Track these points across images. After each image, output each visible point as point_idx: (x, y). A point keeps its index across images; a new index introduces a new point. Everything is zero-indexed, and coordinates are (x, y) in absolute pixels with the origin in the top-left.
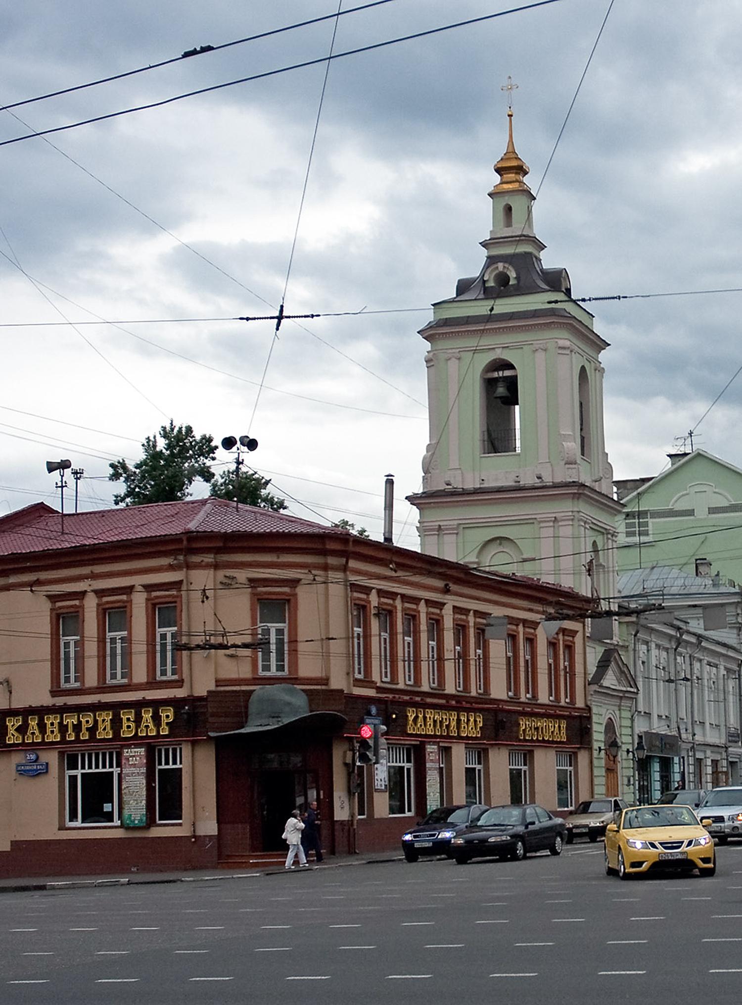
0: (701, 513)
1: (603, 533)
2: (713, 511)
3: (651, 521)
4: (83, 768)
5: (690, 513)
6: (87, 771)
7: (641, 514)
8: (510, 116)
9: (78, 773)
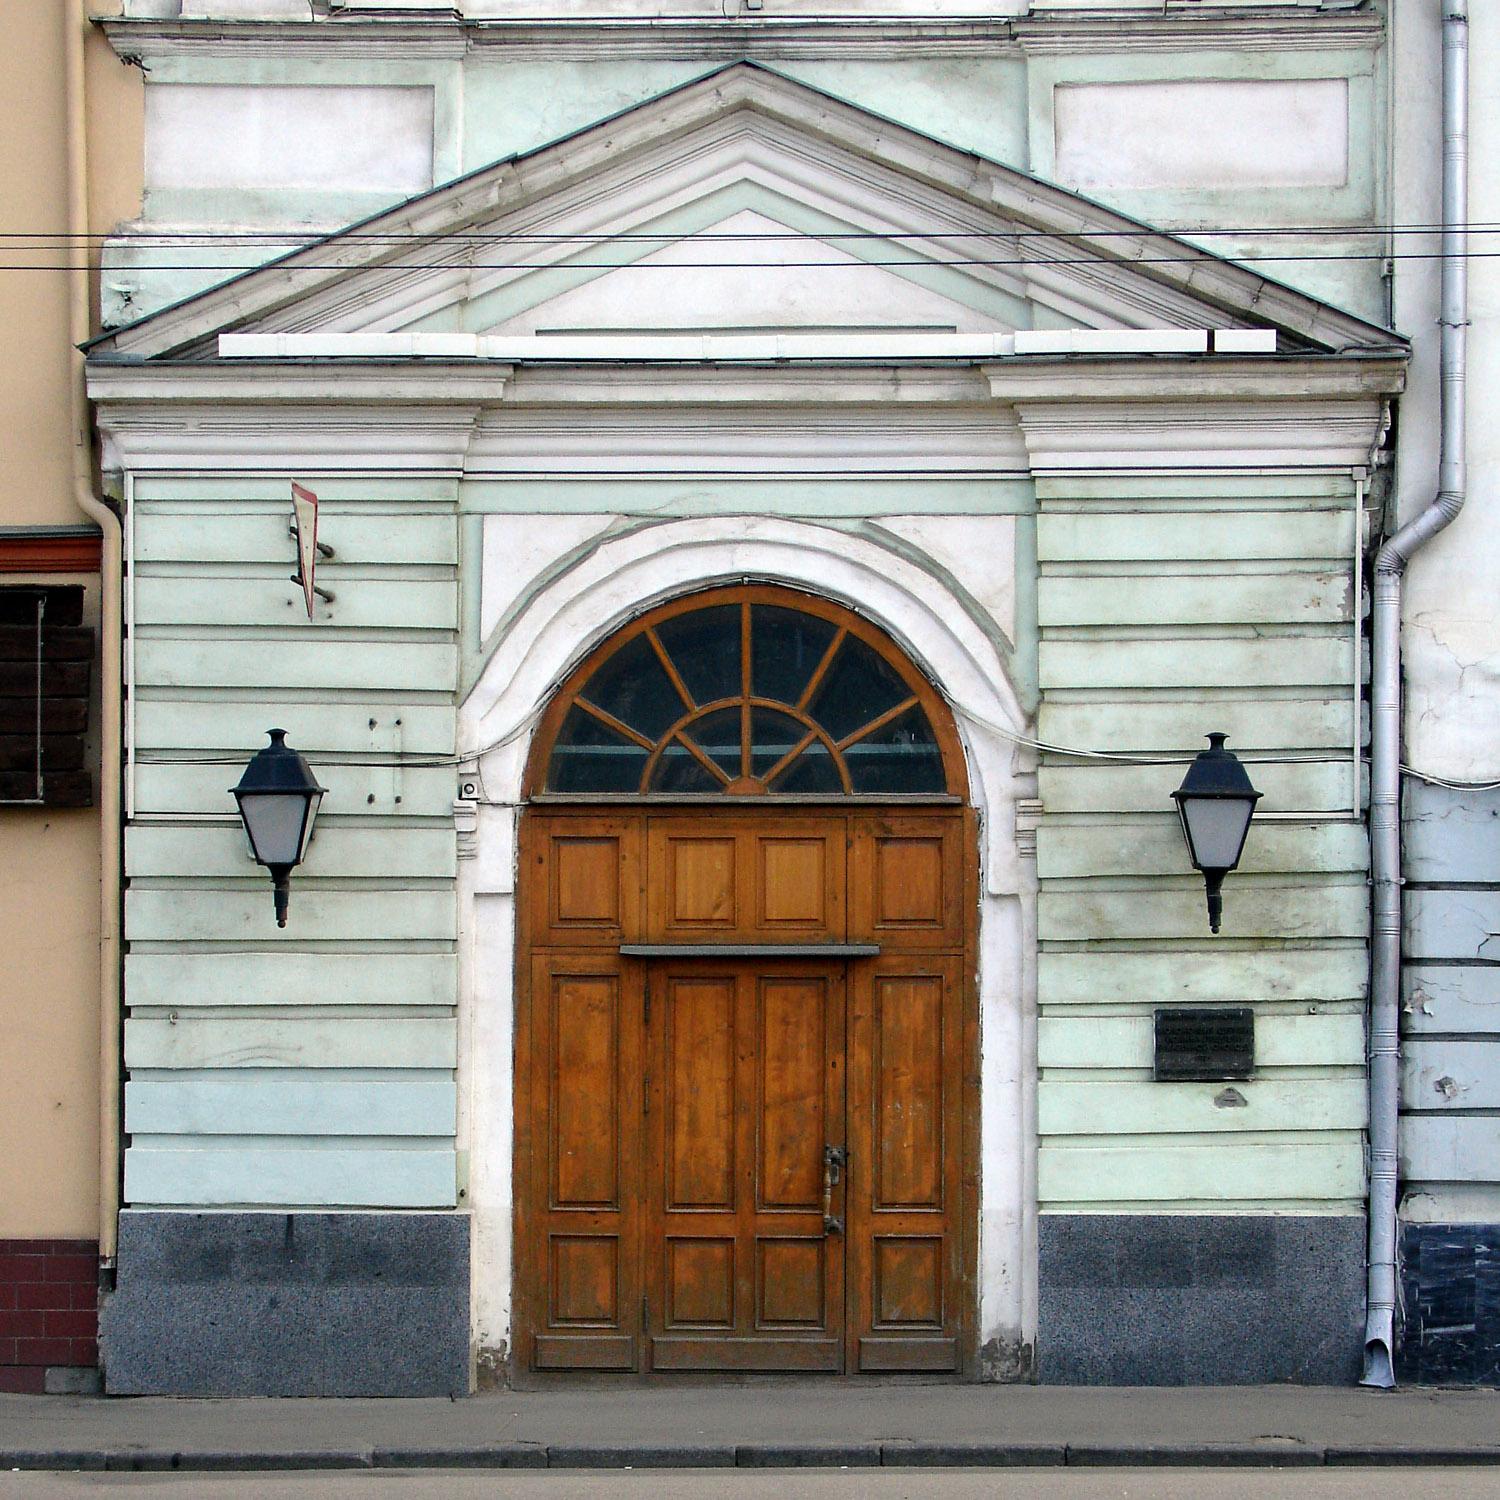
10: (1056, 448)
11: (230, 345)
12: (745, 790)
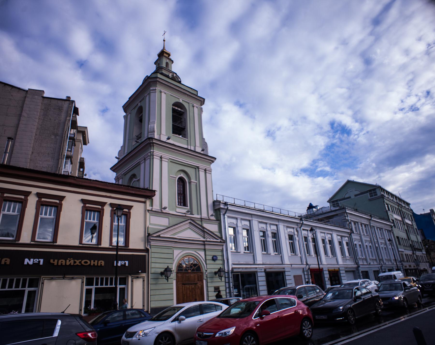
0: (353, 197)
1: (195, 168)
2: (356, 196)
3: (339, 202)
4: (97, 284)
5: (350, 197)
6: (99, 286)
7: (337, 201)
8: (164, 41)
9: (93, 287)
10: (207, 247)
11: (161, 236)
12: (189, 271)
